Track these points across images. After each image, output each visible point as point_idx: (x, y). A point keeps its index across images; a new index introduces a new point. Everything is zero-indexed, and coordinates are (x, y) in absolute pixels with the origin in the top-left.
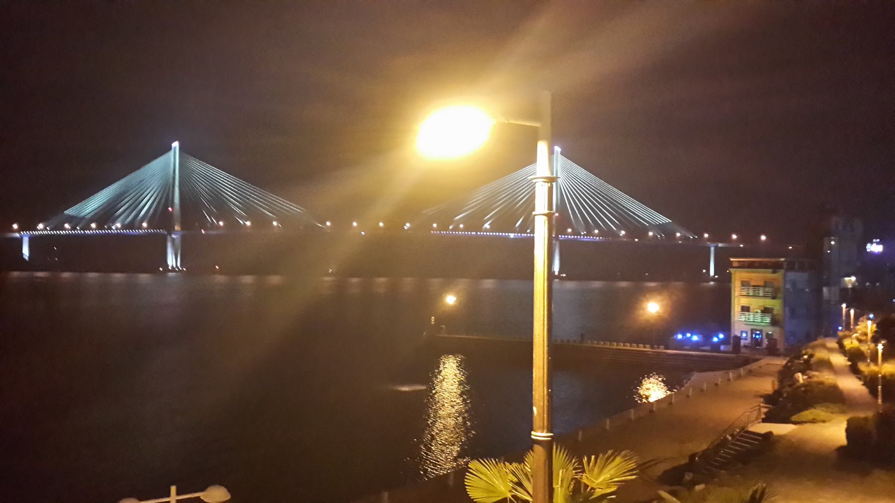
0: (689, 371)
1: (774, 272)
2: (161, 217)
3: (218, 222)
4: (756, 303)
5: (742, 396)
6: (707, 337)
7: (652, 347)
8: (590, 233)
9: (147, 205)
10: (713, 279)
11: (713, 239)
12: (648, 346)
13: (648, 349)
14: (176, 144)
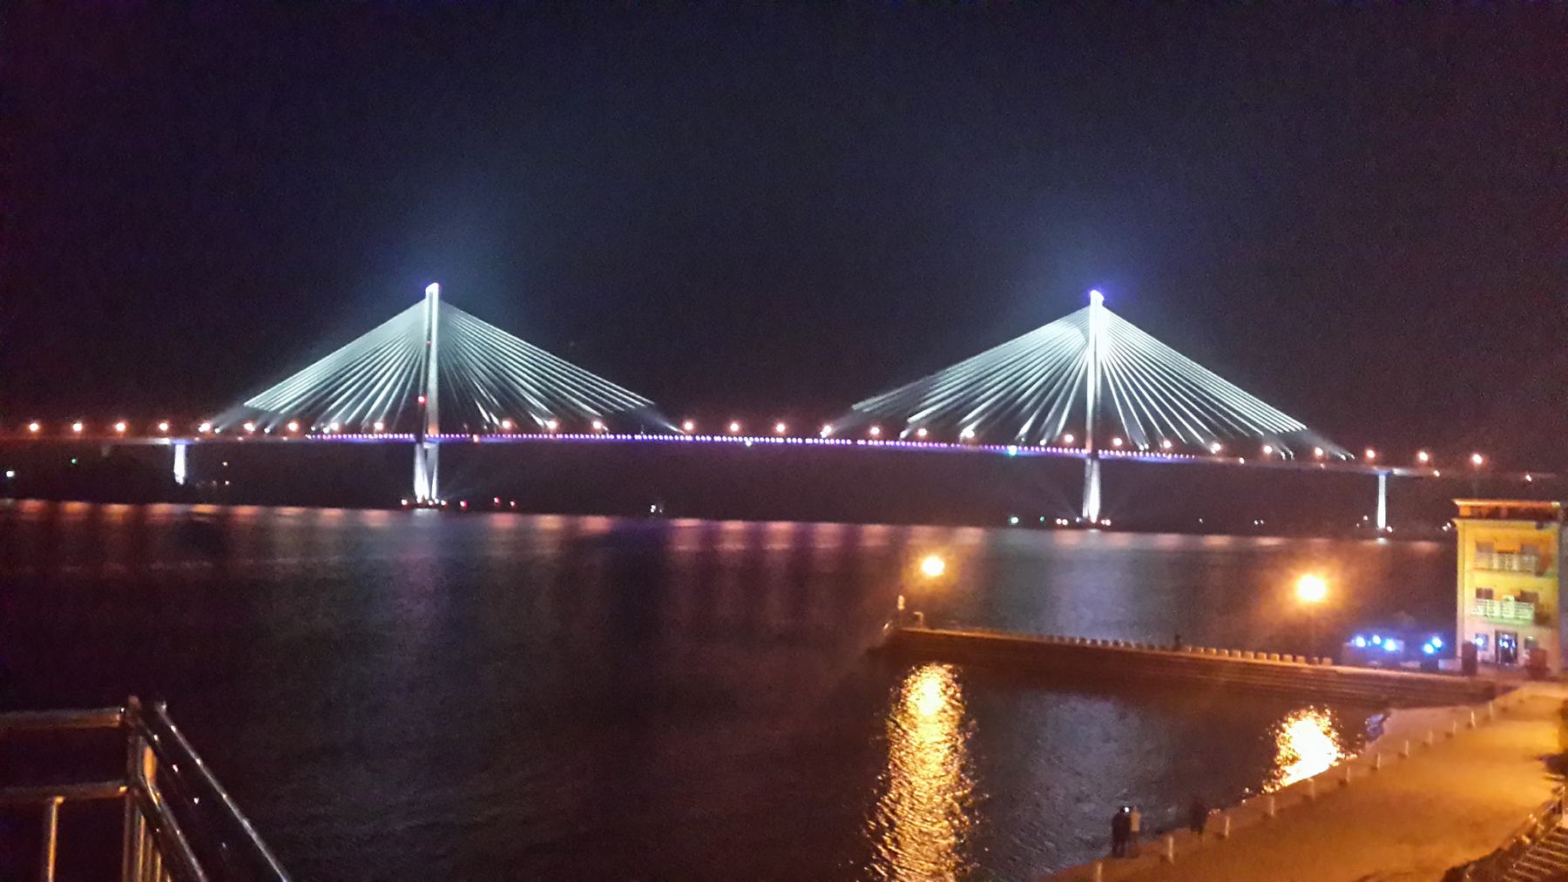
0: (1381, 706)
1: (1540, 527)
2: (407, 416)
3: (197, 433)
4: (1506, 584)
5: (1496, 757)
6: (1413, 646)
7: (1309, 661)
8: (1154, 447)
9: (385, 392)
10: (1385, 534)
11: (1386, 461)
12: (1301, 658)
13: (1301, 663)
14: (433, 290)
